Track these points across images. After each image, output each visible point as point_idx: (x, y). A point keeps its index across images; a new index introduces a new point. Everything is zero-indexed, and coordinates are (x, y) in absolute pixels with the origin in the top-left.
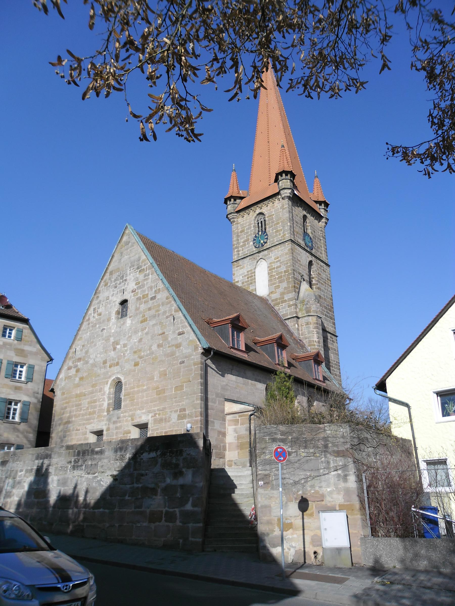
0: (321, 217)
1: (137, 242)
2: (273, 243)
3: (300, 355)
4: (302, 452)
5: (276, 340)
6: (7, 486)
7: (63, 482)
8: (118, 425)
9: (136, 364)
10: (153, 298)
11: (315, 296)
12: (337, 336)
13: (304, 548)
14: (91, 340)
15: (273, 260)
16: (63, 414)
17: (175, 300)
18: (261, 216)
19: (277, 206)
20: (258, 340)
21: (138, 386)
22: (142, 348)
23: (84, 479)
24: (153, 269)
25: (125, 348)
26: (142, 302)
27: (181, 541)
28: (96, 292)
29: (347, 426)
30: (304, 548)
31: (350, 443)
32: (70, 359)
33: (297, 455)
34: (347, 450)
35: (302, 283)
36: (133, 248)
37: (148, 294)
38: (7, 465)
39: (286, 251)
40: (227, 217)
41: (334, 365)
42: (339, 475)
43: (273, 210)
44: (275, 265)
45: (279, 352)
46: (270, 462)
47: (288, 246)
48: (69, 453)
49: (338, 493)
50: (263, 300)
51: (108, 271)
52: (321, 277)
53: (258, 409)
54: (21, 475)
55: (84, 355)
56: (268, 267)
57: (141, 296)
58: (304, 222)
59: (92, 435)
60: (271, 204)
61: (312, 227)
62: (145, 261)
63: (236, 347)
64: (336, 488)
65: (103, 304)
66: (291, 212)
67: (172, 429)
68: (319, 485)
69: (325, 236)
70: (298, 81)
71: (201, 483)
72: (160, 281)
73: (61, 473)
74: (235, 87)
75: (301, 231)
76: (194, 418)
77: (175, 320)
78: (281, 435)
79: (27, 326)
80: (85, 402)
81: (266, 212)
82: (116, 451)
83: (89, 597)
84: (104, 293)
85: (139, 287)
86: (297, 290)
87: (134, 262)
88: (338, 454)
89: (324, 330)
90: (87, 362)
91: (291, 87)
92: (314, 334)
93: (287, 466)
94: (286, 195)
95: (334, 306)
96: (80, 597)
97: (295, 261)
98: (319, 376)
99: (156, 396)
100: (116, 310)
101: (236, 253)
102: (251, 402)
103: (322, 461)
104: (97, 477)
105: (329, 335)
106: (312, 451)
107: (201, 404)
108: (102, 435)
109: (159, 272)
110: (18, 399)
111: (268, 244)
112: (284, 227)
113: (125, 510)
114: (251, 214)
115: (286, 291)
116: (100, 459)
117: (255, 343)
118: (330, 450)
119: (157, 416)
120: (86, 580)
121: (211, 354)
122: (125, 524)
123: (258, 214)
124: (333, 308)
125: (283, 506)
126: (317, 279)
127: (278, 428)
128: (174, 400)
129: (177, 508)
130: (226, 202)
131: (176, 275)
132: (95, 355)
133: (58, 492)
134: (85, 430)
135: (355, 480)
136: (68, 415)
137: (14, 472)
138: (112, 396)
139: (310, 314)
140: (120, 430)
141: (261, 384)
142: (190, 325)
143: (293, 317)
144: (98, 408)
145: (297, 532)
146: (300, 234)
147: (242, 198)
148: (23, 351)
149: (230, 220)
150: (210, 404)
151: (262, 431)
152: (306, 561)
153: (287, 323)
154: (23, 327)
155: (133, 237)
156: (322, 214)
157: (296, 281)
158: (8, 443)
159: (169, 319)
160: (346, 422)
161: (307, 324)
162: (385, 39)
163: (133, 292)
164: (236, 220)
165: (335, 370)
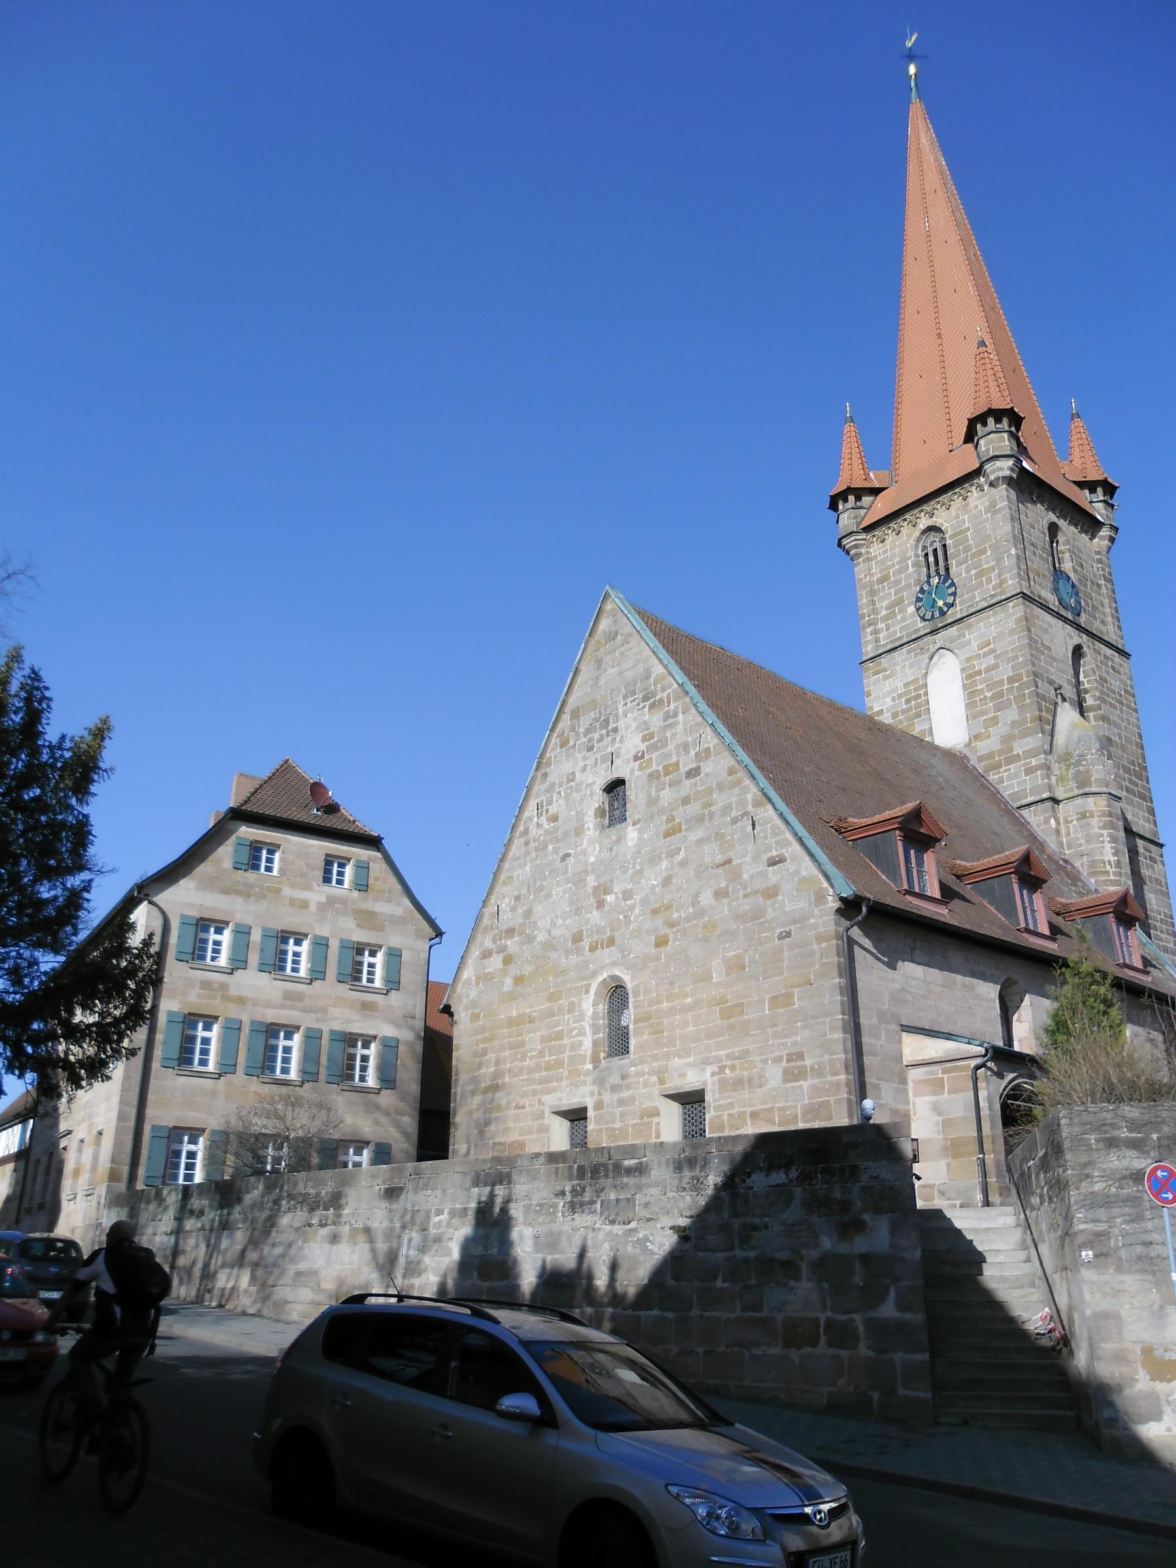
1: (638, 631)
2: (972, 606)
3: (1074, 901)
5: (1015, 867)
6: (409, 1248)
7: (551, 1242)
8: (626, 1094)
9: (661, 942)
10: (693, 773)
11: (1099, 739)
12: (1161, 846)
14: (535, 882)
15: (974, 651)
16: (480, 1066)
18: (934, 537)
20: (966, 868)
21: (670, 998)
23: (601, 1236)
24: (687, 699)
25: (628, 902)
27: (876, 1396)
28: (539, 763)
32: (486, 930)
35: (1059, 709)
36: (626, 647)
37: (677, 764)
38: (402, 1198)
39: (1011, 624)
40: (840, 545)
41: (1158, 924)
43: (966, 517)
45: (1025, 896)
46: (1105, 1201)
47: (1016, 610)
48: (557, 1170)
50: (953, 758)
51: (567, 709)
52: (1108, 688)
54: (440, 1222)
55: (521, 920)
56: (963, 670)
57: (660, 768)
58: (1052, 542)
59: (558, 1119)
60: (958, 502)
62: (664, 679)
63: (917, 890)
65: (559, 793)
66: (1016, 519)
67: (769, 1106)
69: (1110, 574)
72: (709, 729)
73: (540, 1220)
75: (1046, 568)
76: (829, 1078)
77: (758, 828)
78: (1131, 1131)
79: (379, 855)
80: (533, 1039)
81: (946, 525)
82: (679, 1167)
84: (561, 766)
85: (652, 745)
86: (1048, 727)
87: (635, 683)
89: (1128, 831)
90: (530, 939)
92: (1103, 842)
93: (1155, 1211)
94: (1001, 474)
97: (1037, 649)
99: (719, 1022)
100: (597, 805)
101: (870, 638)
102: (967, 1033)
104: (635, 1230)
107: (845, 1041)
108: (585, 1118)
109: (703, 706)
110: (371, 1032)
111: (958, 608)
112: (999, 560)
113: (715, 1314)
114: (904, 531)
115: (1016, 731)
116: (639, 1188)
117: (958, 877)
119: (727, 1071)
121: (861, 911)
122: (722, 1349)
123: (924, 532)
124: (1145, 768)
126: (1097, 694)
127: (1118, 1112)
128: (770, 1031)
129: (856, 1311)
130: (833, 506)
131: (740, 710)
132: (549, 919)
133: (539, 1263)
134: (540, 1107)
136: (493, 1069)
137: (422, 1213)
138: (601, 1022)
139: (1087, 790)
140: (631, 1108)
141: (987, 984)
142: (800, 841)
143: (1042, 801)
146: (1044, 576)
147: (875, 492)
148: (372, 914)
149: (848, 552)
150: (866, 1039)
151: (1076, 1120)
154: (369, 857)
155: (625, 618)
156: (1099, 517)
157: (1044, 703)
159: (739, 824)
161: (1083, 816)
163: (636, 758)
164: (863, 551)
165: (1164, 936)
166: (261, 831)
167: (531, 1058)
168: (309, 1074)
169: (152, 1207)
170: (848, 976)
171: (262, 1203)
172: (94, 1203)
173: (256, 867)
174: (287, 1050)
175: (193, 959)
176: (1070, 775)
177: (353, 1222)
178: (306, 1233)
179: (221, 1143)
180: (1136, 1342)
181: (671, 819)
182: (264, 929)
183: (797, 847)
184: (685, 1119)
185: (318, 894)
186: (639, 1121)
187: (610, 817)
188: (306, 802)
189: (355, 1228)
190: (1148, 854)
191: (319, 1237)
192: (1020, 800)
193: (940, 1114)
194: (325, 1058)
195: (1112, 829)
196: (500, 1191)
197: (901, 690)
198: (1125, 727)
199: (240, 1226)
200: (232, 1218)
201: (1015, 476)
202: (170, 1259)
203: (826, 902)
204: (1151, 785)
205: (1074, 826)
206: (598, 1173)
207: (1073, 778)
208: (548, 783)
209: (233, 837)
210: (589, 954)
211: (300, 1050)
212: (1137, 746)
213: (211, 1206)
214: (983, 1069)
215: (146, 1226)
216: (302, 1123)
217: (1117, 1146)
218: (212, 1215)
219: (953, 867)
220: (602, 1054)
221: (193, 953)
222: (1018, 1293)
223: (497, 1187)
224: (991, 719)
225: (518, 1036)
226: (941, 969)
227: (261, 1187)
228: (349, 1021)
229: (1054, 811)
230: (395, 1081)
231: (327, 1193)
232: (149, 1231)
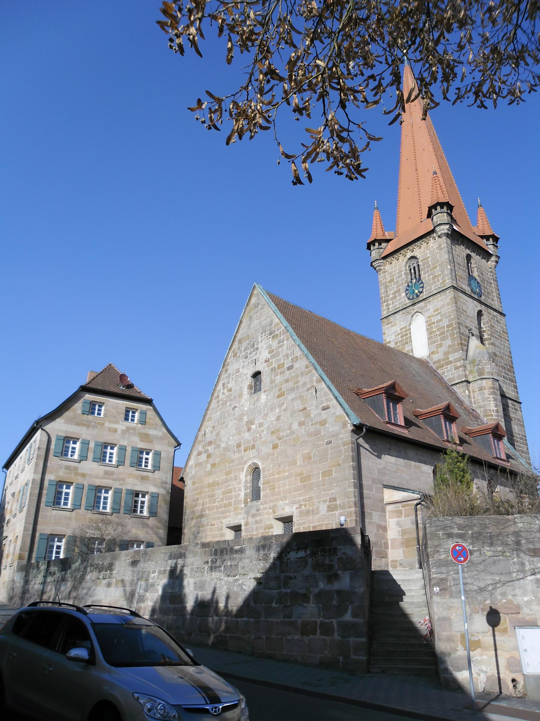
0: (490, 255)
1: (268, 303)
2: (430, 292)
3: (474, 428)
4: (488, 551)
6: (140, 590)
7: (201, 586)
8: (258, 518)
9: (275, 447)
10: (290, 368)
11: (489, 353)
12: (520, 403)
13: (498, 673)
14: (221, 420)
15: (432, 313)
16: (195, 506)
17: (316, 369)
18: (414, 261)
19: (433, 247)
20: (420, 412)
21: (279, 473)
24: (288, 334)
25: (261, 429)
27: (341, 658)
28: (224, 364)
30: (498, 673)
32: (200, 442)
33: (480, 554)
35: (470, 339)
36: (263, 310)
37: (284, 363)
38: (138, 565)
39: (448, 300)
41: (519, 440)
43: (428, 252)
47: (450, 294)
50: (421, 362)
51: (237, 340)
52: (494, 330)
54: (154, 576)
55: (215, 438)
56: (426, 322)
57: (276, 366)
58: (468, 263)
59: (229, 530)
60: (424, 245)
61: (479, 268)
62: (278, 325)
63: (393, 422)
65: (233, 378)
66: (451, 252)
67: (321, 523)
68: (512, 593)
71: (361, 589)
72: (297, 348)
73: (197, 575)
75: (465, 275)
76: (348, 510)
77: (318, 393)
78: (459, 530)
79: (151, 408)
80: (219, 493)
82: (258, 550)
84: (233, 365)
85: (273, 355)
89: (503, 396)
90: (218, 446)
92: (490, 401)
93: (469, 568)
94: (443, 232)
97: (460, 312)
100: (249, 384)
101: (385, 308)
102: (416, 489)
103: (514, 563)
105: (510, 402)
106: (499, 549)
107: (355, 492)
108: (241, 530)
109: (295, 337)
110: (145, 490)
111: (425, 294)
112: (442, 271)
113: (271, 619)
114: (400, 259)
116: (241, 559)
117: (416, 416)
118: (524, 548)
119: (303, 507)
120: (236, 702)
121: (363, 431)
122: (274, 636)
123: (409, 259)
125: (468, 619)
126: (489, 333)
127: (453, 521)
128: (322, 487)
129: (334, 618)
130: (369, 248)
131: (315, 339)
132: (227, 437)
133: (195, 597)
136: (201, 507)
138: (249, 484)
139: (483, 377)
142: (336, 398)
143: (462, 382)
145: (488, 652)
146: (464, 279)
147: (388, 241)
148: (147, 435)
149: (375, 269)
150: (365, 492)
151: (433, 524)
152: (503, 691)
156: (490, 252)
157: (463, 337)
158: (137, 540)
159: (310, 391)
161: (481, 389)
163: (266, 361)
164: (382, 268)
166: (90, 396)
167: (218, 502)
168: (116, 510)
169: (35, 571)
170: (357, 461)
171: (79, 568)
172: (12, 570)
173: (93, 413)
174: (106, 498)
175: (62, 456)
176: (475, 370)
177: (117, 577)
179: (73, 541)
180: (457, 632)
181: (280, 389)
182: (96, 442)
183: (335, 401)
184: (285, 530)
185: (122, 426)
186: (264, 531)
187: (254, 389)
188: (118, 383)
189: (118, 580)
190: (513, 407)
191: (102, 584)
193: (400, 527)
194: (124, 502)
195: (494, 395)
198: (503, 348)
199: (70, 579)
200: (67, 576)
201: (450, 233)
202: (40, 596)
203: (347, 427)
205: (477, 394)
206: (223, 553)
207: (476, 372)
208: (228, 374)
210: (243, 453)
211: (111, 498)
212: (509, 357)
213: (58, 570)
214: (420, 505)
215: (32, 580)
216: (110, 533)
217: (453, 537)
218: (58, 575)
219: (415, 411)
220: (249, 500)
221: (62, 453)
222: (418, 609)
223: (179, 560)
225: (212, 492)
226: (404, 459)
227: (79, 561)
228: (135, 485)
229: (468, 387)
230: (157, 513)
231: (107, 564)
232: (33, 583)
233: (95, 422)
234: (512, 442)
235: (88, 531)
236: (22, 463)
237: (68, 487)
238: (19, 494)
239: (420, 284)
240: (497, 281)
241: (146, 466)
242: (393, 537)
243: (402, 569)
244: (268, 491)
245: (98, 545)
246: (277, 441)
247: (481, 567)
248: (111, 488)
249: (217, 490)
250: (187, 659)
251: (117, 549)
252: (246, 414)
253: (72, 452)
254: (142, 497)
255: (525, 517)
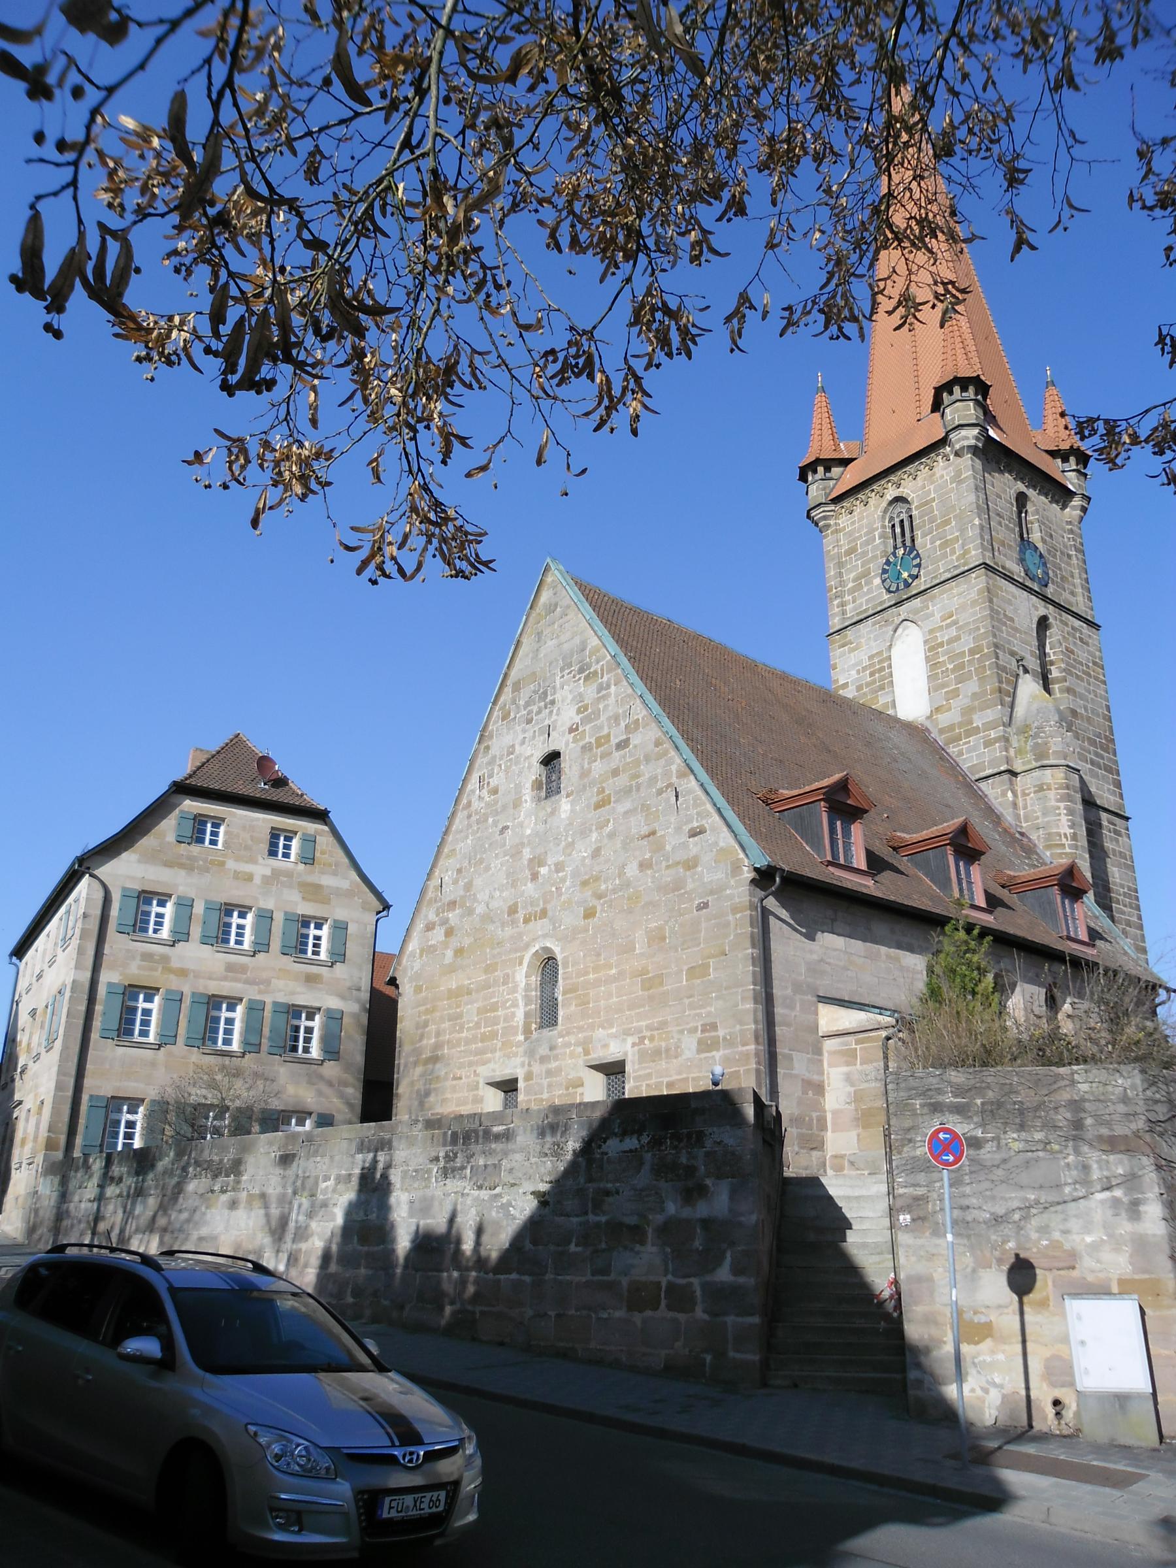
0: (1070, 494)
2: (935, 577)
4: (1014, 1140)
7: (423, 1207)
8: (553, 1065)
9: (589, 914)
10: (622, 745)
11: (1059, 712)
12: (1127, 819)
13: (1028, 1388)
14: (475, 855)
16: (422, 1037)
17: (677, 747)
18: (900, 508)
19: (942, 476)
21: (596, 969)
22: (601, 872)
23: (469, 1201)
24: (619, 671)
26: (596, 756)
27: (708, 1358)
28: (482, 735)
29: (1136, 1071)
30: (1028, 1388)
31: (1144, 1118)
32: (430, 902)
33: (999, 1147)
34: (1137, 1134)
35: (1020, 681)
36: (565, 619)
37: (609, 735)
38: (295, 1164)
39: (973, 594)
42: (1116, 1202)
43: (932, 487)
44: (942, 636)
47: (979, 580)
49: (1117, 1250)
50: (913, 730)
51: (509, 682)
52: (1075, 660)
53: (904, 1023)
55: (462, 893)
56: (926, 642)
57: (593, 740)
58: (1020, 513)
59: (492, 1090)
60: (924, 472)
61: (1044, 524)
62: (598, 651)
63: (842, 861)
64: (1109, 1236)
65: (500, 766)
66: (981, 488)
67: (684, 1076)
68: (1061, 1227)
69: (1082, 544)
70: (805, 306)
71: (752, 1215)
72: (638, 701)
73: (416, 1185)
74: (599, 404)
76: (740, 1048)
78: (956, 1096)
79: (326, 828)
80: (470, 1010)
82: (542, 1134)
83: (464, 1483)
84: (502, 738)
85: (586, 717)
86: (1008, 699)
88: (1113, 1144)
89: (1089, 803)
90: (470, 912)
91: (790, 324)
92: (1059, 814)
93: (973, 1176)
94: (966, 443)
95: (1116, 737)
96: (445, 1480)
97: (999, 621)
98: (1076, 928)
101: (837, 610)
102: (890, 1005)
103: (1068, 1165)
105: (1104, 816)
106: (1038, 1136)
107: (755, 1011)
108: (516, 1090)
109: (634, 678)
110: (317, 1005)
111: (923, 579)
112: (963, 531)
113: (568, 1278)
114: (872, 502)
116: (505, 1153)
117: (895, 849)
118: (1090, 1134)
119: (646, 1042)
120: (456, 1443)
122: (572, 1312)
123: (891, 503)
128: (687, 1001)
129: (695, 1276)
130: (803, 478)
131: (678, 682)
132: (487, 892)
133: (414, 1228)
135: (1161, 1216)
138: (534, 993)
142: (719, 811)
144: (502, 1025)
145: (1006, 1347)
146: (1010, 547)
147: (845, 462)
148: (318, 888)
149: (817, 524)
150: (779, 1010)
151: (903, 1085)
153: (984, 789)
157: (1004, 675)
158: (298, 1108)
159: (664, 795)
160: (1137, 1059)
161: (1040, 788)
162: (1014, 178)
163: (571, 730)
164: (832, 522)
167: (469, 1029)
168: (251, 1046)
169: (79, 1175)
172: (34, 1172)
173: (201, 841)
174: (230, 1021)
177: (250, 1188)
178: (209, 1199)
179: (160, 1111)
182: (207, 902)
183: (716, 818)
185: (263, 867)
191: (220, 1204)
192: (978, 772)
193: (852, 1085)
196: (382, 1157)
197: (866, 663)
204: (1118, 758)
209: (177, 811)
211: (242, 1022)
213: (129, 1173)
215: (73, 1193)
216: (242, 1093)
217: (942, 1111)
218: (130, 1181)
219: (893, 838)
220: (534, 1026)
221: (134, 925)
224: (952, 691)
226: (864, 940)
227: (172, 1154)
228: (293, 993)
232: (76, 1198)
233: (205, 861)
234: (1105, 903)
235: (193, 1091)
236: (50, 945)
237: (149, 999)
238: (45, 1012)
239: (913, 559)
240: (1083, 552)
241: (315, 953)
242: (837, 1106)
243: (854, 1173)
244: (573, 1008)
245: (215, 1118)
246: (594, 902)
247: (1000, 1172)
248: (241, 1000)
249: (467, 1004)
250: (364, 1359)
251: (256, 1128)
252: (529, 843)
253: (157, 923)
254: (308, 1019)
255: (1095, 1071)
